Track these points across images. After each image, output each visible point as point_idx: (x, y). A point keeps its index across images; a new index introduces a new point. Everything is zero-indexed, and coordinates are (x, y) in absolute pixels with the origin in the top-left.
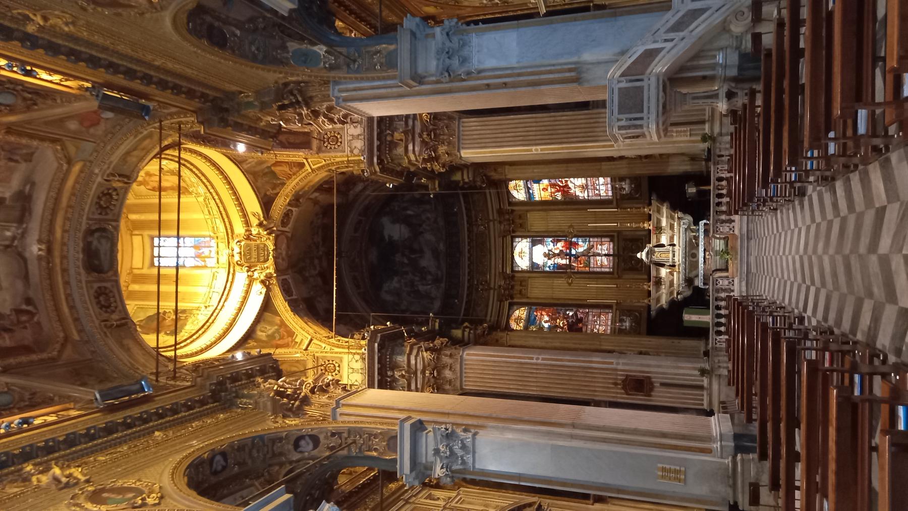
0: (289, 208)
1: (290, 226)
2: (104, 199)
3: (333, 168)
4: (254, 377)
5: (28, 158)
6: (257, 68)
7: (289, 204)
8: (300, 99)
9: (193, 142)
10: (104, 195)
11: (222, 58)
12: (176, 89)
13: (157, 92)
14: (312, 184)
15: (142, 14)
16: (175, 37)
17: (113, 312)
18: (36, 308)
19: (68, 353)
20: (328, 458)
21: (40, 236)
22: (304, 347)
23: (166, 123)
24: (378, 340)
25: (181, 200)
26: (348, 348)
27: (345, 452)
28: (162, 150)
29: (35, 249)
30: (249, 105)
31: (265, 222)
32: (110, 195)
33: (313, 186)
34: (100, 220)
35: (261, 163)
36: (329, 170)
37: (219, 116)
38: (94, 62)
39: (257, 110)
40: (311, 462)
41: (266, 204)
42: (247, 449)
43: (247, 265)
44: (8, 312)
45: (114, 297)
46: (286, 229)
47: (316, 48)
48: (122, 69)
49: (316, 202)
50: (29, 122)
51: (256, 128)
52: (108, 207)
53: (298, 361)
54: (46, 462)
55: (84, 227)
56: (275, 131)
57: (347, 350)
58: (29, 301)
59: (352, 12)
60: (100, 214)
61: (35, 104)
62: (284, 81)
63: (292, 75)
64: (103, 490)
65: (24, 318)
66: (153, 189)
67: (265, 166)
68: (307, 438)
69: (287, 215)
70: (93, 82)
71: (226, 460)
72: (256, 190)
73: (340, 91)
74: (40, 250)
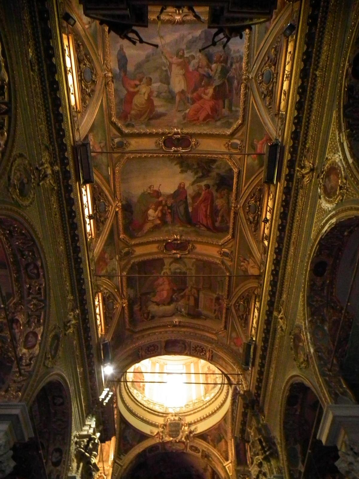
2: (200, 349)
4: (104, 426)
5: (217, 318)
6: (280, 425)
7: (203, 451)
8: (268, 453)
9: (233, 393)
10: (202, 349)
12: (259, 381)
13: (257, 370)
15: (295, 360)
16: (287, 377)
17: (146, 353)
18: (150, 320)
19: (127, 333)
21: (182, 322)
22: (117, 461)
23: (241, 377)
25: (201, 385)
28: (226, 375)
29: (176, 320)
30: (258, 422)
31: (192, 435)
32: (202, 352)
33: (215, 467)
34: (190, 347)
35: (226, 432)
37: (249, 404)
38: (265, 340)
39: (256, 425)
40: (44, 461)
41: (203, 436)
42: (38, 296)
43: (168, 423)
44: (148, 309)
45: (153, 353)
46: (188, 449)
47: (300, 464)
48: (263, 369)
49: (205, 470)
50: (233, 317)
52: (196, 351)
54: (79, 319)
55: (187, 340)
56: (245, 438)
58: (153, 317)
61: (241, 320)
62: (276, 442)
63: (281, 447)
64: (58, 340)
65: (145, 315)
69: (196, 449)
70: (256, 341)
71: (60, 405)
72: (210, 430)
74: (176, 322)
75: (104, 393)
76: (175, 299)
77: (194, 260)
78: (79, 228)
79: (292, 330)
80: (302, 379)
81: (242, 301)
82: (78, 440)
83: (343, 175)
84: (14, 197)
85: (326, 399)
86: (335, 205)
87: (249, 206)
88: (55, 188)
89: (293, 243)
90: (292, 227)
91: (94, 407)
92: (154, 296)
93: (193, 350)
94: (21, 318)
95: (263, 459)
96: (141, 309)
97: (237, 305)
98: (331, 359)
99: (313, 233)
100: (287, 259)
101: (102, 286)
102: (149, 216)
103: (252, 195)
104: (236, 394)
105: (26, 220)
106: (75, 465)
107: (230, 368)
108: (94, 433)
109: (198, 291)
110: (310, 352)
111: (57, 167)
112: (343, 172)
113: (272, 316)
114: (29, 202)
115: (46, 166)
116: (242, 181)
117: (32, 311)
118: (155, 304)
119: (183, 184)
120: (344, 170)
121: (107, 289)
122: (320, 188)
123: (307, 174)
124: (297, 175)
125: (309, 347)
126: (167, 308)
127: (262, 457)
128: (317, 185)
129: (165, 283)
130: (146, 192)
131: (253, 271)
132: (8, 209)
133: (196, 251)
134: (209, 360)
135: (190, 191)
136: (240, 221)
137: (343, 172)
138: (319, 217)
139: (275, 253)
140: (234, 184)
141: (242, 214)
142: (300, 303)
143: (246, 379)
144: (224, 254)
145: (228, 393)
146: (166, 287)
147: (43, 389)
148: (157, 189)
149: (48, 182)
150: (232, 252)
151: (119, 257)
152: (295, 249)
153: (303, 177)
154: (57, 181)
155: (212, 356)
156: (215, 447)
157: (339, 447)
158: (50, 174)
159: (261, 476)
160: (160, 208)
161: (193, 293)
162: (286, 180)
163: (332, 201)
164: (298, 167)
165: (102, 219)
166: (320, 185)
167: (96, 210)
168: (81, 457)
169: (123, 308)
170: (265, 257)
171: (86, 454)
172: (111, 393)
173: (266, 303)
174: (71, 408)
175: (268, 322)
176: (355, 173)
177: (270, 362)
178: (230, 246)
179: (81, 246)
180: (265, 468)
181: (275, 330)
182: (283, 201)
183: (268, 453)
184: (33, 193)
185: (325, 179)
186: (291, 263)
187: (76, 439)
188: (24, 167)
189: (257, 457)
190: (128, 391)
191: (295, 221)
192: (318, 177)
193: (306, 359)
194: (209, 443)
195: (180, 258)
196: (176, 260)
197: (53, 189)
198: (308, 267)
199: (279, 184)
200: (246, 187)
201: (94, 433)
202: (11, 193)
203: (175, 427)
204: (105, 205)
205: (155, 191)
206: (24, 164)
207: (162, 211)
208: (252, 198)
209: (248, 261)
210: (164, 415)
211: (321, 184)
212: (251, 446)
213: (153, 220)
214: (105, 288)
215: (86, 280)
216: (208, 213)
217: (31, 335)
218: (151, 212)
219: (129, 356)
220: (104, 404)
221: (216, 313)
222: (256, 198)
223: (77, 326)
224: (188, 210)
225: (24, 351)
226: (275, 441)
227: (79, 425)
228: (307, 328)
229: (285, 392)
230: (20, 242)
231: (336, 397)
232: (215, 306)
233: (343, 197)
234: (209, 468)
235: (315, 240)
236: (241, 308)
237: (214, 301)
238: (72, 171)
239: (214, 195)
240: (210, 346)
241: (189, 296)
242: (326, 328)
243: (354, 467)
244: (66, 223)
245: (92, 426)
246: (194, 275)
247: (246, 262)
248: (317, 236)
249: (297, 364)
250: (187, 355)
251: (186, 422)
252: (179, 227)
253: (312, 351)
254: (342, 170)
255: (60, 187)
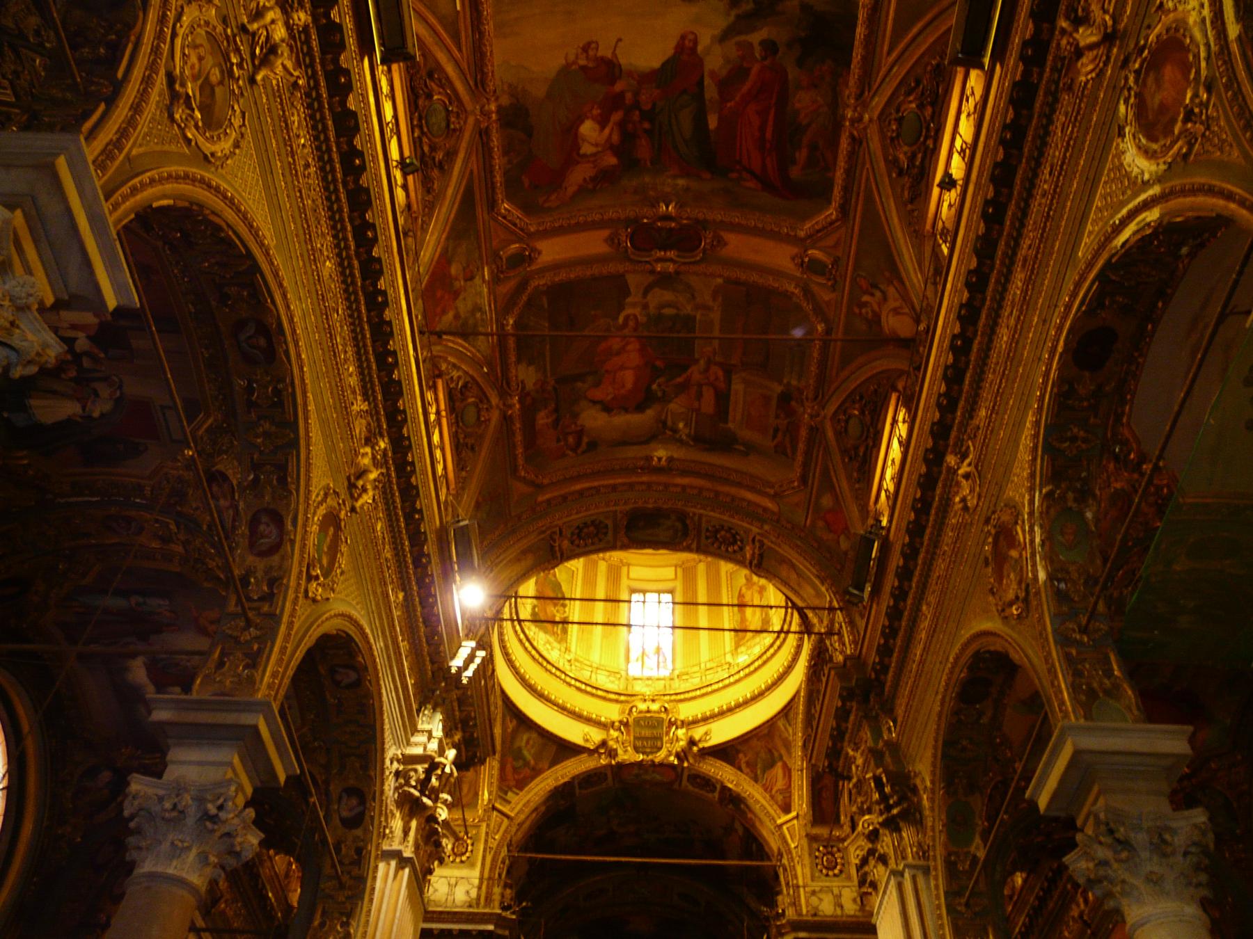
0: (718, 787)
1: (690, 787)
3: (785, 861)
4: (464, 731)
6: (935, 748)
7: (724, 788)
8: (895, 811)
10: (734, 536)
11: (944, 697)
12: (890, 632)
14: (758, 824)
15: (992, 592)
16: (966, 634)
17: (572, 543)
18: (583, 452)
20: (324, 841)
22: (497, 805)
24: (500, 932)
26: (490, 878)
27: (327, 870)
29: (661, 453)
30: (877, 734)
31: (695, 749)
32: (734, 543)
33: (754, 826)
35: (788, 745)
36: (780, 854)
38: (915, 530)
41: (725, 752)
44: (579, 423)
45: (593, 544)
47: (978, 840)
51: (843, 739)
53: (476, 794)
54: (386, 462)
55: (691, 510)
57: (486, 875)
58: (593, 445)
59: (1042, 900)
60: (707, 530)
62: (920, 787)
63: (932, 800)
64: (338, 528)
65: (571, 439)
66: (741, 596)
67: (783, 752)
68: (360, 808)
69: (707, 783)
71: (349, 686)
73: (914, 878)
74: (660, 459)
75: (463, 653)
76: (659, 394)
77: (720, 281)
78: (376, 203)
79: (994, 512)
80: (1007, 645)
81: (857, 406)
82: (401, 768)
83: (1204, 73)
84: (190, 136)
85: (1062, 703)
86: (1163, 167)
87: (900, 121)
88: (300, 82)
89: (1025, 260)
90: (1024, 212)
91: (435, 686)
92: (597, 384)
93: (707, 538)
94: (234, 472)
95: (884, 824)
96: (556, 422)
97: (842, 417)
98: (1092, 600)
99: (1086, 240)
100: (1000, 307)
101: (446, 360)
102: (584, 140)
103: (908, 85)
104: (819, 659)
105: (231, 202)
106: (397, 824)
107: (812, 591)
108: (441, 752)
109: (728, 371)
110: (1036, 577)
111: (302, 15)
112: (1203, 64)
113: (941, 465)
114: (231, 141)
115: (270, 16)
116: (884, 36)
117: (261, 452)
118: (598, 407)
119: (691, 37)
120: (1208, 59)
121: (458, 368)
122: (1126, 101)
123: (1091, 47)
124: (1058, 44)
125: (1034, 565)
126: (635, 419)
127: (881, 820)
128: (1116, 90)
129: (630, 347)
130: (574, 63)
131: (897, 324)
132: (177, 178)
133: (725, 252)
134: (751, 563)
135: (715, 61)
136: (868, 166)
137: (1203, 64)
138: (1110, 194)
139: (968, 285)
140: (856, 43)
141: (875, 144)
142: (1026, 441)
143: (851, 623)
144: (814, 267)
145: (799, 648)
146: (633, 357)
147: (309, 652)
148: (609, 55)
149: (279, 70)
150: (836, 261)
151: (491, 272)
152: (1027, 282)
153: (1079, 52)
154: (303, 58)
155: (761, 556)
156: (756, 780)
157: (1079, 823)
158: (283, 41)
159: (872, 862)
160: (616, 117)
161: (712, 378)
162: (1022, 58)
163: (1155, 152)
164: (1067, 18)
165: (439, 156)
166: (1126, 93)
167: (421, 127)
168: (411, 806)
169: (506, 419)
170: (936, 292)
171: (425, 800)
172: (481, 654)
173: (927, 428)
174: (380, 694)
175: (928, 483)
176: (1242, 74)
177: (923, 586)
178: (830, 241)
179: (384, 257)
180: (887, 843)
181: (946, 504)
182: (1005, 127)
183: (895, 811)
184: (238, 111)
185: (1147, 73)
186: (1012, 322)
187: (395, 765)
188: (207, 32)
189: (867, 817)
190: (522, 636)
191: (1038, 193)
192: (1125, 63)
193: (1022, 595)
194: (740, 769)
195: (677, 273)
196: (665, 280)
197: (295, 85)
198: (1058, 341)
199: (998, 67)
200: (894, 55)
201: (441, 752)
202: (179, 126)
203: (649, 729)
204: (447, 110)
205: (602, 59)
206: (207, 23)
207: (621, 125)
208: (909, 93)
209: (883, 293)
210: (623, 697)
211: (1130, 89)
212: (854, 791)
213: (594, 155)
214: (454, 366)
215: (400, 355)
216: (768, 135)
217: (264, 519)
218: (588, 128)
219: (524, 552)
220: (465, 681)
221: (780, 435)
222: (923, 94)
223: (384, 487)
224: (707, 125)
225: (251, 559)
226: (918, 781)
227: (401, 733)
228: (1037, 514)
229: (957, 670)
230: (213, 261)
231: (1089, 699)
232: (777, 417)
233: (1191, 146)
234: (737, 825)
235: (1090, 265)
236: (854, 428)
237: (774, 403)
238: (349, 24)
239: (790, 77)
240: (755, 530)
241: (700, 386)
242: (1089, 515)
243: (1110, 872)
244: (336, 190)
245: (434, 734)
246: (716, 333)
247: (878, 294)
248: (1096, 255)
249: (996, 605)
250: (688, 549)
251: (682, 717)
252: (675, 177)
253: (1042, 575)
254: (1203, 55)
255: (314, 76)
